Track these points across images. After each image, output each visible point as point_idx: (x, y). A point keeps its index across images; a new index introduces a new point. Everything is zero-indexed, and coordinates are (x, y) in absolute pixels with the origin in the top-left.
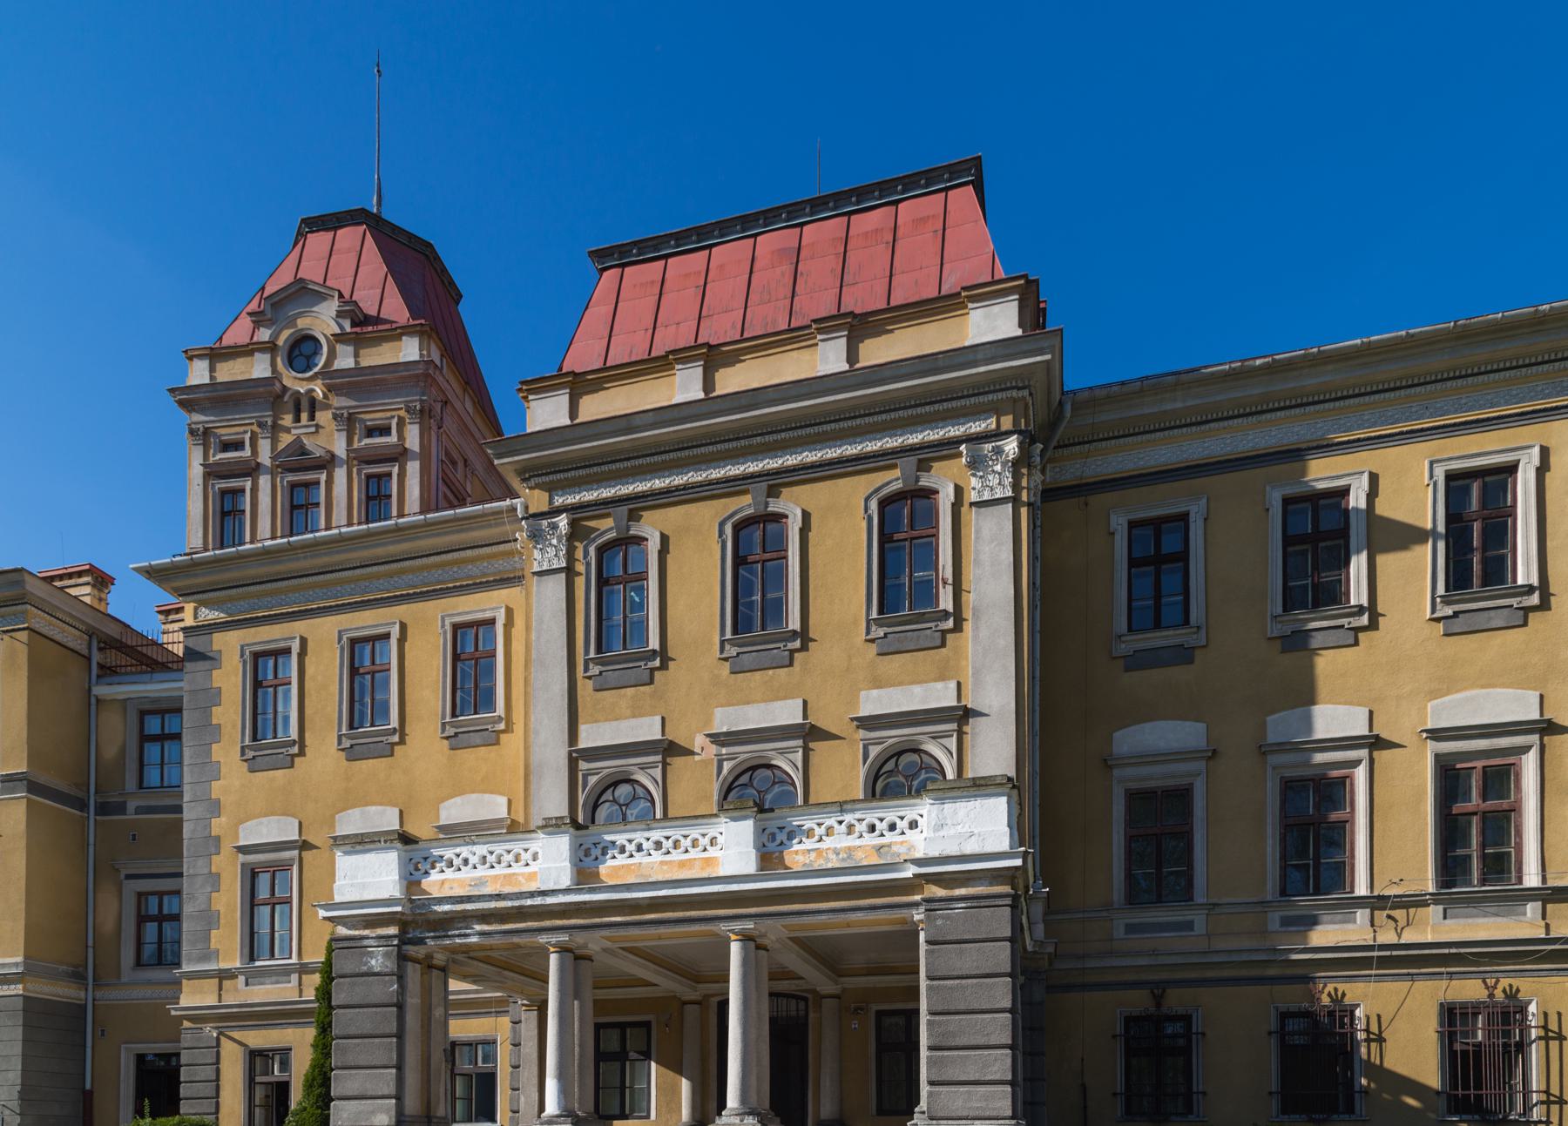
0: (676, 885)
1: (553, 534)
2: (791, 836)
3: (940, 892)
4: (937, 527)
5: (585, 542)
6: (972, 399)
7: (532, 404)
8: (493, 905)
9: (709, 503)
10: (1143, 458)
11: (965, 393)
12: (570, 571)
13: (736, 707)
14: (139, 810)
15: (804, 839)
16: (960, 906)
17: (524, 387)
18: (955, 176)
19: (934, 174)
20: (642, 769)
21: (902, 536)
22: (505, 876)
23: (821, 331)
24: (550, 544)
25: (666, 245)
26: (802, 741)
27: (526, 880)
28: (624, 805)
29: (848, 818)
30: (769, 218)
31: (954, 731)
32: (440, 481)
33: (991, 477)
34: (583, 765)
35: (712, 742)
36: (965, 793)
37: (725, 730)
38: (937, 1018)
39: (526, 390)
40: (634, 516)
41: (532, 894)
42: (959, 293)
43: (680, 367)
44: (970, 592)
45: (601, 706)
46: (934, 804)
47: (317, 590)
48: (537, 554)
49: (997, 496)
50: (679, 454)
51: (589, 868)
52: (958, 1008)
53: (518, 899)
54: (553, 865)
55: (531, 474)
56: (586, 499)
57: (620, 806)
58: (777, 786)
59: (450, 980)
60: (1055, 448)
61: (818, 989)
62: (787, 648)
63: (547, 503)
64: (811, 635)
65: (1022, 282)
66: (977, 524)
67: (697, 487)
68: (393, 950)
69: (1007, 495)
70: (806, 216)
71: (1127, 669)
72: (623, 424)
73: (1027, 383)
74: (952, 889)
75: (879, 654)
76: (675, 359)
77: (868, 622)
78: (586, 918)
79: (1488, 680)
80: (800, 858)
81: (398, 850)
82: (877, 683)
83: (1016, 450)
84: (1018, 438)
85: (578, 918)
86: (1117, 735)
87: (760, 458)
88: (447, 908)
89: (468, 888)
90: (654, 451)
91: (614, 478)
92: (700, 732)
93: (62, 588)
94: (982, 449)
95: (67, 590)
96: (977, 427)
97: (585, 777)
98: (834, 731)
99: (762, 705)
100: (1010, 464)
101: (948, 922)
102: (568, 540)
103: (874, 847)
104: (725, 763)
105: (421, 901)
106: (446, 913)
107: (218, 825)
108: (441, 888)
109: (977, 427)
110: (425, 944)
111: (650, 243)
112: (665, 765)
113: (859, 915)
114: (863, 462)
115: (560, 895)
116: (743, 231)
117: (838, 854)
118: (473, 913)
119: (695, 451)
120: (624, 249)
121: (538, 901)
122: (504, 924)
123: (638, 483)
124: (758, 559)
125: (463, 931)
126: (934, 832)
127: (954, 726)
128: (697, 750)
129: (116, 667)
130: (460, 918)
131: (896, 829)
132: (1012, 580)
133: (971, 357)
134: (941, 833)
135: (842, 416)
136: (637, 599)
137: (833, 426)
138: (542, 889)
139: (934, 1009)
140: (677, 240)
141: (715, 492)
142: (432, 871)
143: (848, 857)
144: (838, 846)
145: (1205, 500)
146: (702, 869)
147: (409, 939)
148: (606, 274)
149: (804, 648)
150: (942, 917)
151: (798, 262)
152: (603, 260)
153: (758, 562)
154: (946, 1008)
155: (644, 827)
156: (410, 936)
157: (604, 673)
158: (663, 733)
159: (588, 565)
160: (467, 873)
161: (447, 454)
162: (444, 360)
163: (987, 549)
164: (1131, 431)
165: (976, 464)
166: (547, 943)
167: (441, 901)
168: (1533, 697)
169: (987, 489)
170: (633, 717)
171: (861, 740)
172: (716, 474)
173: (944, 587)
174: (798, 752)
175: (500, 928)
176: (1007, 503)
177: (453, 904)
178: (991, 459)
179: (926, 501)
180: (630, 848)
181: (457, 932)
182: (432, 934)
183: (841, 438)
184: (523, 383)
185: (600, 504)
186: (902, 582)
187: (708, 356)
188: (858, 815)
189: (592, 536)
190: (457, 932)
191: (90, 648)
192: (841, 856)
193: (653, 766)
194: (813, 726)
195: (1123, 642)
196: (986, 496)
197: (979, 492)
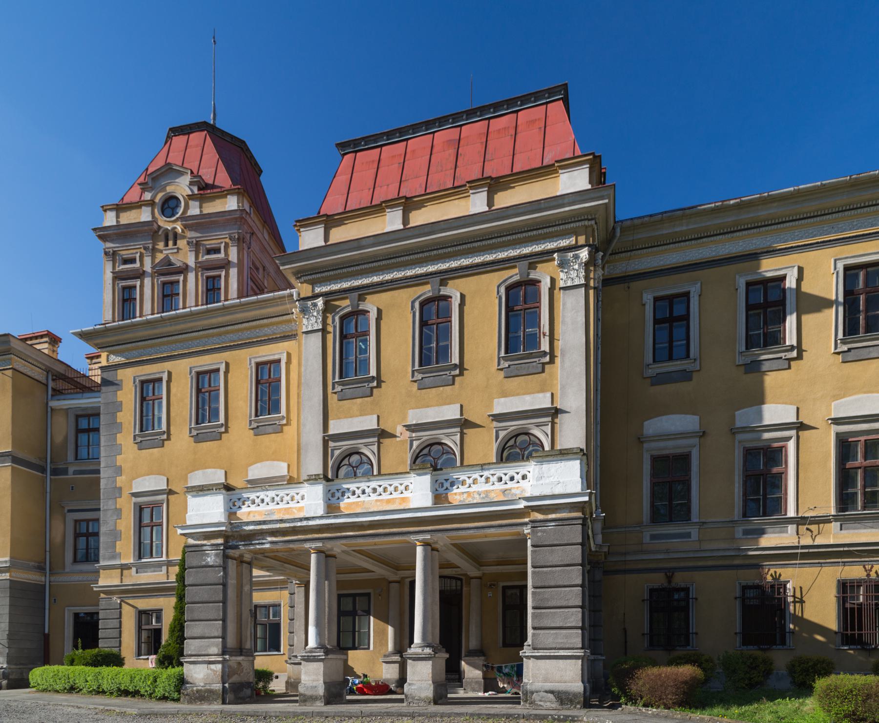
0: (385, 513)
3: (540, 517)
6: (561, 227)
7: (302, 233)
8: (278, 526)
9: (406, 290)
14: (76, 472)
15: (460, 486)
16: (551, 524)
17: (298, 224)
18: (552, 95)
19: (541, 94)
21: (519, 308)
22: (286, 509)
23: (471, 188)
29: (486, 473)
31: (549, 422)
32: (249, 279)
33: (572, 272)
35: (407, 430)
36: (555, 458)
38: (538, 590)
39: (299, 226)
40: (362, 298)
41: (301, 520)
42: (554, 164)
43: (389, 210)
47: (178, 344)
48: (305, 321)
49: (576, 284)
50: (388, 262)
53: (293, 522)
56: (511, 255)
57: (353, 467)
58: (531, 446)
59: (254, 570)
60: (611, 254)
61: (468, 573)
62: (540, 362)
64: (465, 366)
65: (591, 157)
66: (564, 300)
68: (220, 553)
70: (463, 120)
71: (653, 385)
72: (355, 244)
73: (593, 217)
75: (505, 377)
76: (386, 206)
77: (499, 358)
80: (458, 497)
81: (223, 494)
82: (504, 394)
86: (646, 423)
88: (251, 527)
89: (264, 516)
90: (373, 260)
93: (31, 345)
95: (35, 346)
96: (564, 243)
97: (333, 451)
98: (481, 424)
99: (436, 408)
100: (583, 264)
102: (323, 313)
103: (501, 490)
104: (414, 442)
107: (121, 481)
109: (564, 243)
110: (239, 548)
111: (372, 138)
112: (379, 443)
117: (480, 495)
118: (268, 531)
120: (357, 142)
121: (304, 523)
125: (261, 541)
127: (549, 419)
128: (398, 435)
129: (62, 390)
133: (560, 202)
134: (541, 482)
135: (484, 238)
136: (363, 347)
137: (479, 243)
139: (536, 585)
140: (387, 136)
141: (409, 283)
142: (243, 507)
143: (486, 497)
144: (480, 490)
147: (230, 546)
148: (346, 157)
150: (541, 531)
155: (366, 479)
158: (378, 425)
159: (335, 327)
161: (253, 263)
162: (252, 209)
163: (569, 315)
165: (563, 265)
167: (248, 524)
172: (410, 273)
173: (544, 338)
176: (582, 287)
178: (572, 262)
179: (534, 287)
180: (358, 492)
181: (257, 542)
182: (243, 543)
184: (297, 221)
185: (342, 292)
188: (492, 472)
189: (337, 310)
190: (257, 542)
191: (47, 379)
192: (481, 496)
194: (466, 420)
195: (651, 369)
196: (569, 284)
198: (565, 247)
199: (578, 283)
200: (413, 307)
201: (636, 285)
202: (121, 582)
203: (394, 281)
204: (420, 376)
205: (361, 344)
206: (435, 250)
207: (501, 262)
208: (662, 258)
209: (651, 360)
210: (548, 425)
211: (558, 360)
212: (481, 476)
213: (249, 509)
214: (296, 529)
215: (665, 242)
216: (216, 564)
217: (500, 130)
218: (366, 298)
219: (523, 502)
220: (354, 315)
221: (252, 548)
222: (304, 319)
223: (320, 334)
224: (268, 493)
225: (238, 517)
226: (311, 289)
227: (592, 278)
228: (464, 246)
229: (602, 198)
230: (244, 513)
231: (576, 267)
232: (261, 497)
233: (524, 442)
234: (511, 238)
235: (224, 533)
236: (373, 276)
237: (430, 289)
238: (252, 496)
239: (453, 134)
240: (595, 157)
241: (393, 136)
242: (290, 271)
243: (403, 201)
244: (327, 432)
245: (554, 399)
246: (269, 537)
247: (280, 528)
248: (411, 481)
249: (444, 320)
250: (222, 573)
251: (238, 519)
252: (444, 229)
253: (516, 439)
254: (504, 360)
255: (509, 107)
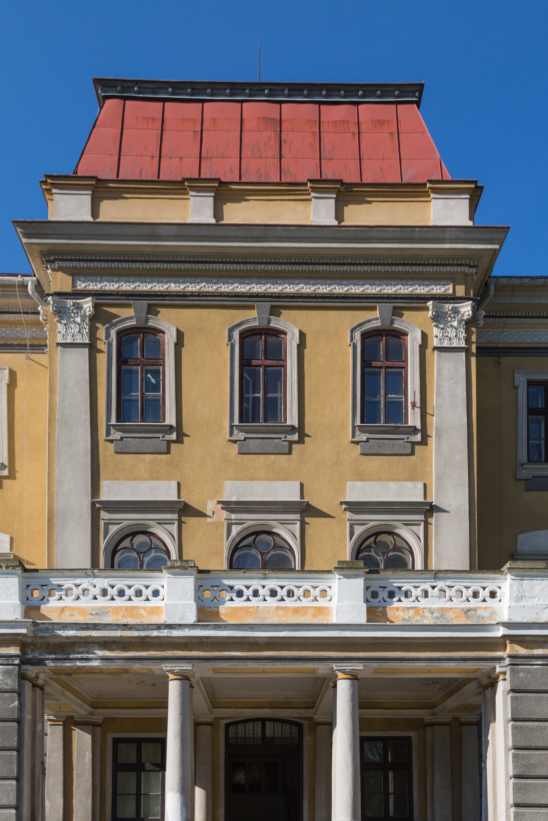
0: (296, 628)
1: (454, 317)
2: (391, 595)
3: (522, 651)
4: (406, 361)
5: (107, 325)
6: (435, 268)
7: (55, 197)
8: (118, 633)
9: (219, 311)
10: (537, 336)
11: (431, 262)
12: (92, 348)
13: (243, 482)
15: (403, 599)
16: (538, 663)
17: (49, 181)
19: (389, 89)
20: (160, 524)
21: (378, 364)
22: (127, 608)
23: (314, 189)
24: (74, 321)
25: (337, 93)
26: (299, 515)
27: (147, 613)
28: (142, 553)
29: (440, 584)
30: (253, 90)
31: (422, 521)
33: (449, 330)
34: (104, 515)
35: (223, 508)
36: (541, 574)
37: (234, 499)
38: (521, 752)
39: (51, 184)
40: (152, 310)
41: (159, 627)
42: (425, 184)
43: (194, 193)
44: (433, 416)
45: (122, 466)
46: (515, 580)
48: (60, 327)
49: (454, 345)
50: (193, 266)
51: (209, 607)
52: (538, 745)
53: (144, 630)
54: (180, 602)
55: (57, 257)
56: (368, 291)
58: (154, 550)
62: (409, 440)
63: (71, 286)
64: (306, 431)
65: (473, 186)
66: (438, 364)
67: (210, 296)
68: (13, 670)
69: (462, 346)
70: (284, 96)
71: (527, 490)
72: (148, 230)
73: (476, 263)
74: (531, 649)
75: (362, 454)
76: (189, 186)
77: (354, 427)
78: (207, 651)
80: (400, 614)
81: (19, 576)
82: (361, 477)
83: (91, 308)
84: (472, 304)
85: (199, 651)
86: (520, 537)
87: (263, 282)
88: (71, 633)
89: (88, 617)
90: (171, 259)
91: (134, 275)
92: (212, 499)
94: (443, 308)
96: (438, 290)
97: (107, 525)
98: (329, 513)
99: (266, 483)
100: (464, 322)
101: (529, 676)
102: (90, 320)
103: (462, 609)
104: (233, 526)
105: (45, 626)
106: (68, 638)
108: (61, 614)
109: (438, 290)
110: (45, 665)
111: (150, 86)
112: (180, 523)
113: (452, 664)
114: (350, 300)
115: (186, 630)
116: (231, 95)
117: (432, 613)
118: (97, 640)
119: (207, 266)
120: (126, 85)
121: (165, 633)
122: (126, 651)
123: (156, 284)
124: (260, 364)
125: (85, 656)
126: (515, 602)
127: (422, 517)
128: (209, 513)
130: (82, 643)
131: (277, 595)
132: (466, 411)
133: (440, 235)
134: (522, 603)
135: (333, 262)
136: (153, 381)
137: (325, 267)
138: (169, 622)
139: (519, 744)
141: (225, 303)
142: (50, 598)
143: (441, 617)
144: (433, 606)
146: (314, 616)
147: (27, 659)
148: (108, 102)
149: (301, 441)
150: (524, 671)
151: (281, 131)
152: (106, 89)
153: (261, 366)
154: (528, 744)
155: (261, 575)
156: (30, 656)
157: (124, 439)
158: (179, 496)
159: (110, 345)
160: (87, 602)
164: (531, 314)
165: (438, 318)
166: (168, 671)
167: (65, 626)
169: (447, 338)
170: (151, 479)
171: (348, 520)
172: (225, 288)
173: (413, 409)
174: (296, 524)
175: (119, 655)
176: (462, 352)
177: (78, 630)
178: (450, 316)
179: (397, 339)
180: (248, 593)
181: (79, 656)
182: (53, 656)
183: (331, 279)
184: (48, 176)
185: (122, 295)
186: (378, 400)
187: (217, 190)
188: (449, 583)
189: (114, 321)
190: (79, 656)
192: (435, 615)
193: (170, 522)
194: (308, 504)
195: (525, 469)
196: (446, 344)
197: (440, 340)
198: (243, 293)
199: (457, 346)
200: (230, 338)
201: (507, 361)
203: (203, 296)
204: (364, 437)
205: (149, 375)
206: (262, 263)
207: (370, 298)
208: (536, 334)
209: (525, 460)
210: (174, 524)
211: (432, 441)
212: (433, 587)
213: (61, 604)
214: (147, 640)
215: (541, 314)
216: (6, 687)
217: (336, 122)
218: (281, 313)
219: (501, 628)
220: (139, 333)
221: (68, 665)
222: (59, 324)
223: (86, 350)
224: (95, 581)
225: (44, 615)
226: (71, 282)
227: (473, 342)
228: (304, 267)
229: (492, 242)
230: (54, 609)
231: (455, 324)
232: (84, 586)
233: (142, 544)
234: (445, 270)
235: (20, 638)
236: (170, 282)
237: (256, 316)
238: (238, 584)
239: (271, 111)
240: (477, 187)
241: (279, 93)
242: (38, 248)
243: (217, 185)
244: (98, 496)
245: (428, 492)
246: (99, 650)
247: (121, 636)
248: (329, 585)
249: (275, 363)
250: (16, 703)
251: (44, 617)
252: (280, 237)
253: (132, 540)
254: (360, 431)
255: (347, 94)
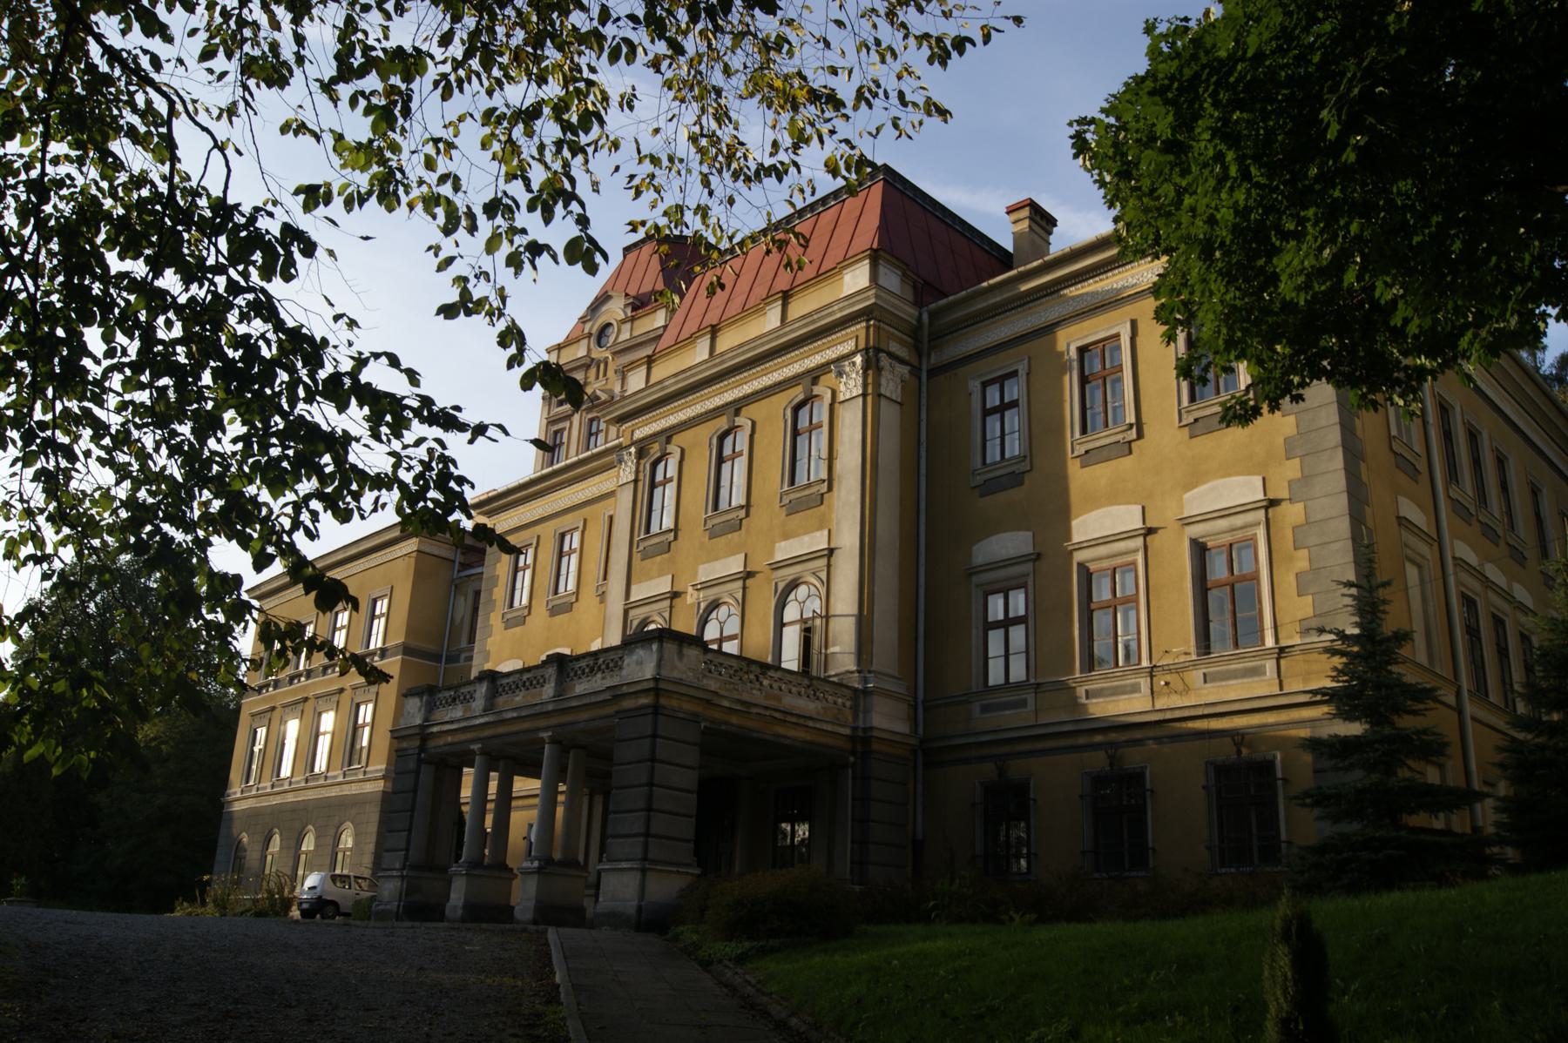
71: (982, 496)
79: (1227, 470)
82: (786, 537)
145: (1026, 362)
168: (1258, 480)
202: (1281, 689)
